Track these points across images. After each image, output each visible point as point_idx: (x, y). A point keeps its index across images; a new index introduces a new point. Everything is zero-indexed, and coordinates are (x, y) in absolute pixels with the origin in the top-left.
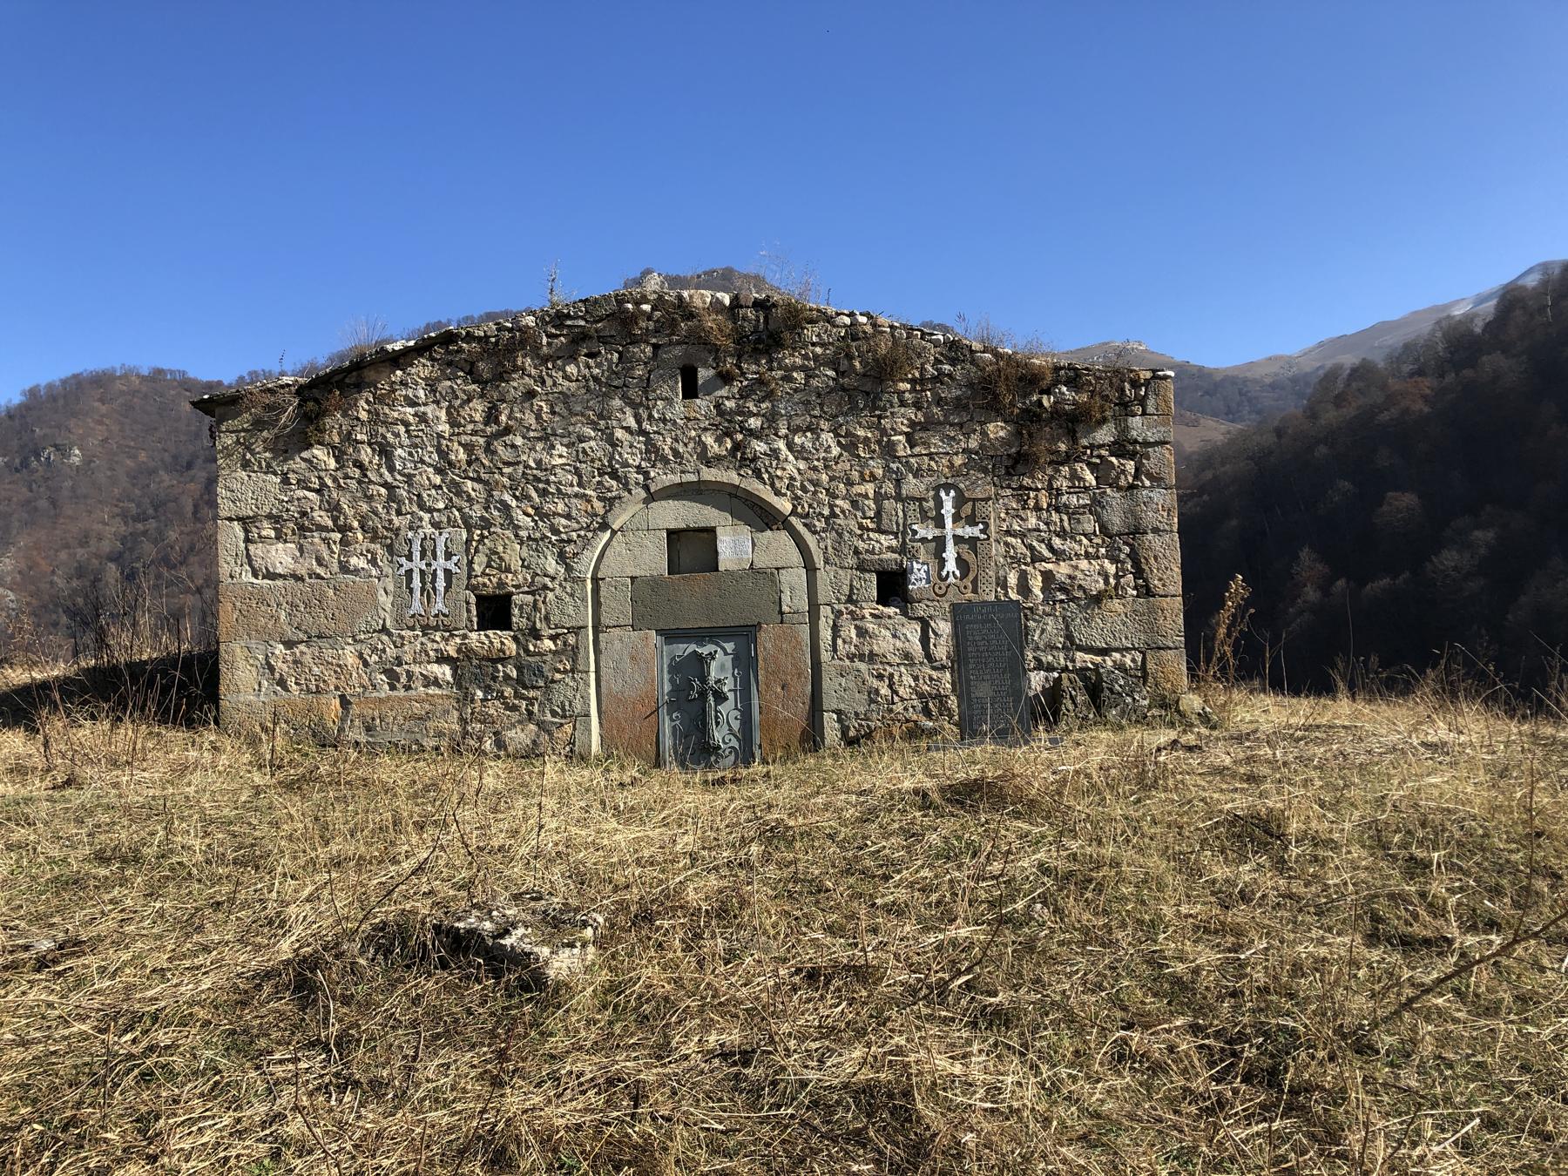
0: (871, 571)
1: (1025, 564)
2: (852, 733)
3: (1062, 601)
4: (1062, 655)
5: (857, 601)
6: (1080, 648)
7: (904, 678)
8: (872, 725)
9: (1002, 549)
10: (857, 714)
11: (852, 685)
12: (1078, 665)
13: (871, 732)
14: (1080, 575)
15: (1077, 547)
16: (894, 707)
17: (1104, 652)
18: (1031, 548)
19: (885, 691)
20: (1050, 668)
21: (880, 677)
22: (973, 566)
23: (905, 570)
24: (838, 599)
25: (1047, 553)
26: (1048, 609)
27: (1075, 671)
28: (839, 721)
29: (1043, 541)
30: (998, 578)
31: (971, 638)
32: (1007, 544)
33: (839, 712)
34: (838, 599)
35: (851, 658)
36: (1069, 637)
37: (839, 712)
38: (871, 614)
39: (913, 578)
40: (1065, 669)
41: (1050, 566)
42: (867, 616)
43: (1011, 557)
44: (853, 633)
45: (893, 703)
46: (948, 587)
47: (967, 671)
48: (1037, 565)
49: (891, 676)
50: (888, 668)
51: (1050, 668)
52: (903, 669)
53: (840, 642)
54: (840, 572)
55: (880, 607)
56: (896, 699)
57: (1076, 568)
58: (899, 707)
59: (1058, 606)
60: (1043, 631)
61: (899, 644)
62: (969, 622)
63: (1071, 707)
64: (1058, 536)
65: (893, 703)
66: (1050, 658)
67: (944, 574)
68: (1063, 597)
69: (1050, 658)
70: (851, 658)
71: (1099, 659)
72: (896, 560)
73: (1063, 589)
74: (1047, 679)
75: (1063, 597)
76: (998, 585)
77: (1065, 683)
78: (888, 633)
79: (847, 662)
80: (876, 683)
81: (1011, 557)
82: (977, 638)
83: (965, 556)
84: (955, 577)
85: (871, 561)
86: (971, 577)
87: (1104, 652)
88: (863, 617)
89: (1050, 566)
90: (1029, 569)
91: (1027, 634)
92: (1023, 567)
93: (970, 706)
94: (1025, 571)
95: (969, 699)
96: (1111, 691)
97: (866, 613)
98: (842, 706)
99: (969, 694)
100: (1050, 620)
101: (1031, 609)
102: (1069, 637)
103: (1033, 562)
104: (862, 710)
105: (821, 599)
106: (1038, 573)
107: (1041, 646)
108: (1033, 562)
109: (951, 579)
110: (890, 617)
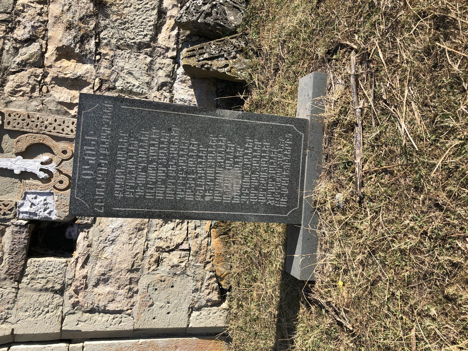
0: (25, 266)
1: (44, 76)
2: (215, 296)
3: (98, 45)
4: (159, 60)
5: (64, 284)
6: (154, 38)
7: (163, 235)
8: (209, 274)
9: (18, 100)
10: (196, 290)
11: (163, 295)
12: (172, 45)
13: (216, 276)
14: (68, 17)
15: (31, 11)
16: (193, 249)
17: (162, 13)
18: (23, 65)
19: (174, 258)
20: (172, 75)
21: (158, 262)
22: (38, 139)
23: (31, 222)
24: (58, 306)
25: (34, 48)
26: (105, 63)
27: (179, 51)
28: (199, 309)
29: (17, 50)
30: (58, 112)
31: (140, 192)
32: (14, 93)
33: (192, 309)
34: (58, 306)
35: (132, 293)
36: (140, 46)
37: (192, 309)
38: (83, 267)
39: (43, 214)
40: (176, 60)
41: (51, 48)
42: (84, 272)
43: (33, 90)
44: (103, 289)
45: (189, 250)
46: (61, 172)
47: (196, 204)
48: (47, 63)
49: (158, 249)
50: (149, 253)
51: (172, 75)
52: (153, 236)
53: (111, 307)
54: (20, 303)
55: (76, 254)
56: (185, 246)
57: (57, 18)
58: (193, 244)
59: (103, 51)
60: (130, 73)
61: (124, 238)
62: (110, 190)
63: (222, 62)
64: (12, 30)
65: (189, 250)
66: (161, 73)
67: (42, 175)
68: (93, 42)
69: (161, 73)
70: (132, 293)
71: (170, 23)
72: (13, 233)
73: (83, 39)
74: (183, 82)
75: (93, 42)
76: (66, 113)
77: (193, 62)
78: (109, 250)
79: (137, 298)
80: (164, 268)
81: (33, 90)
82: (141, 179)
83: (23, 146)
84: (49, 162)
85: (10, 264)
86: (50, 142)
87: (162, 13)
88: (85, 277)
89: (51, 48)
90: (52, 73)
91: (131, 92)
92: (48, 80)
93: (251, 207)
94: (53, 79)
95: (241, 207)
96: (209, 14)
97: (80, 273)
98: (186, 306)
99: (232, 207)
100: (120, 63)
101: (102, 82)
102: (140, 46)
103: (42, 66)
104: (191, 285)
105: (54, 329)
106: (58, 64)
107: (147, 79)
108: (42, 66)
109: (52, 167)
110: (89, 246)
